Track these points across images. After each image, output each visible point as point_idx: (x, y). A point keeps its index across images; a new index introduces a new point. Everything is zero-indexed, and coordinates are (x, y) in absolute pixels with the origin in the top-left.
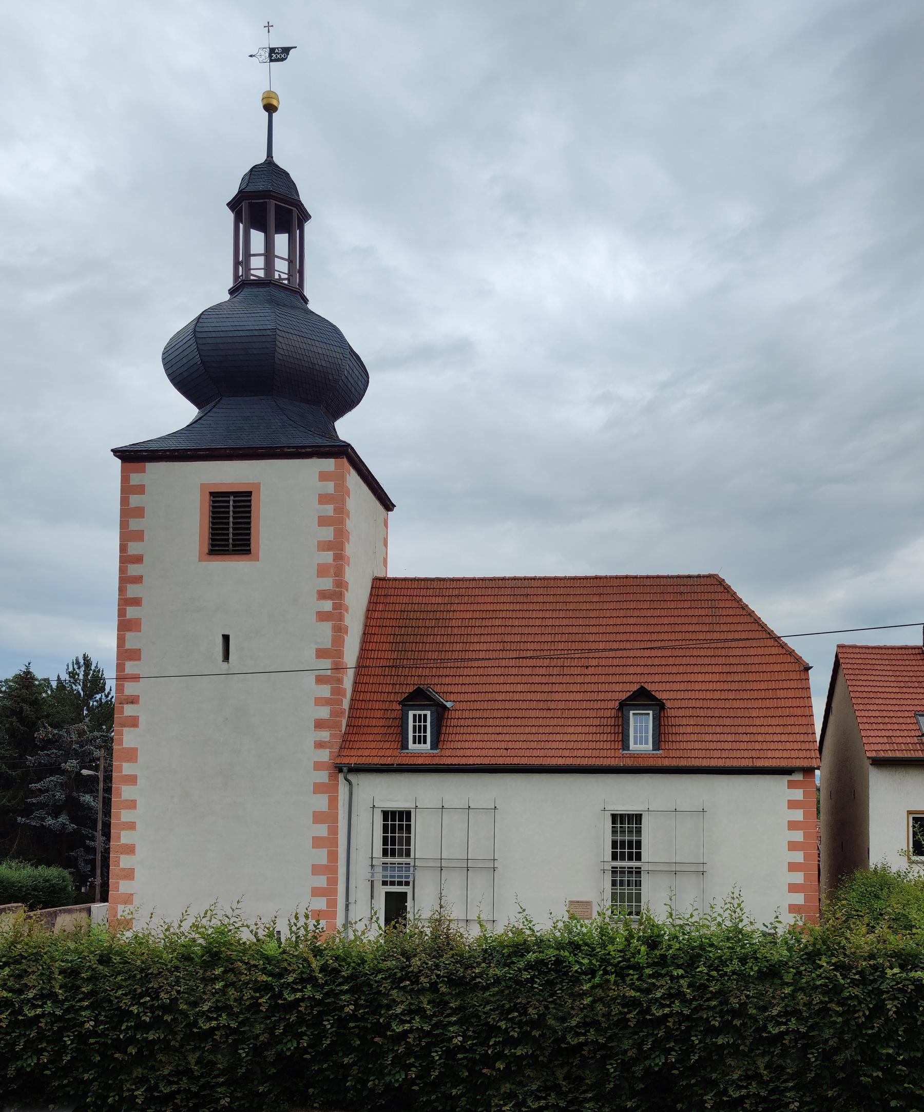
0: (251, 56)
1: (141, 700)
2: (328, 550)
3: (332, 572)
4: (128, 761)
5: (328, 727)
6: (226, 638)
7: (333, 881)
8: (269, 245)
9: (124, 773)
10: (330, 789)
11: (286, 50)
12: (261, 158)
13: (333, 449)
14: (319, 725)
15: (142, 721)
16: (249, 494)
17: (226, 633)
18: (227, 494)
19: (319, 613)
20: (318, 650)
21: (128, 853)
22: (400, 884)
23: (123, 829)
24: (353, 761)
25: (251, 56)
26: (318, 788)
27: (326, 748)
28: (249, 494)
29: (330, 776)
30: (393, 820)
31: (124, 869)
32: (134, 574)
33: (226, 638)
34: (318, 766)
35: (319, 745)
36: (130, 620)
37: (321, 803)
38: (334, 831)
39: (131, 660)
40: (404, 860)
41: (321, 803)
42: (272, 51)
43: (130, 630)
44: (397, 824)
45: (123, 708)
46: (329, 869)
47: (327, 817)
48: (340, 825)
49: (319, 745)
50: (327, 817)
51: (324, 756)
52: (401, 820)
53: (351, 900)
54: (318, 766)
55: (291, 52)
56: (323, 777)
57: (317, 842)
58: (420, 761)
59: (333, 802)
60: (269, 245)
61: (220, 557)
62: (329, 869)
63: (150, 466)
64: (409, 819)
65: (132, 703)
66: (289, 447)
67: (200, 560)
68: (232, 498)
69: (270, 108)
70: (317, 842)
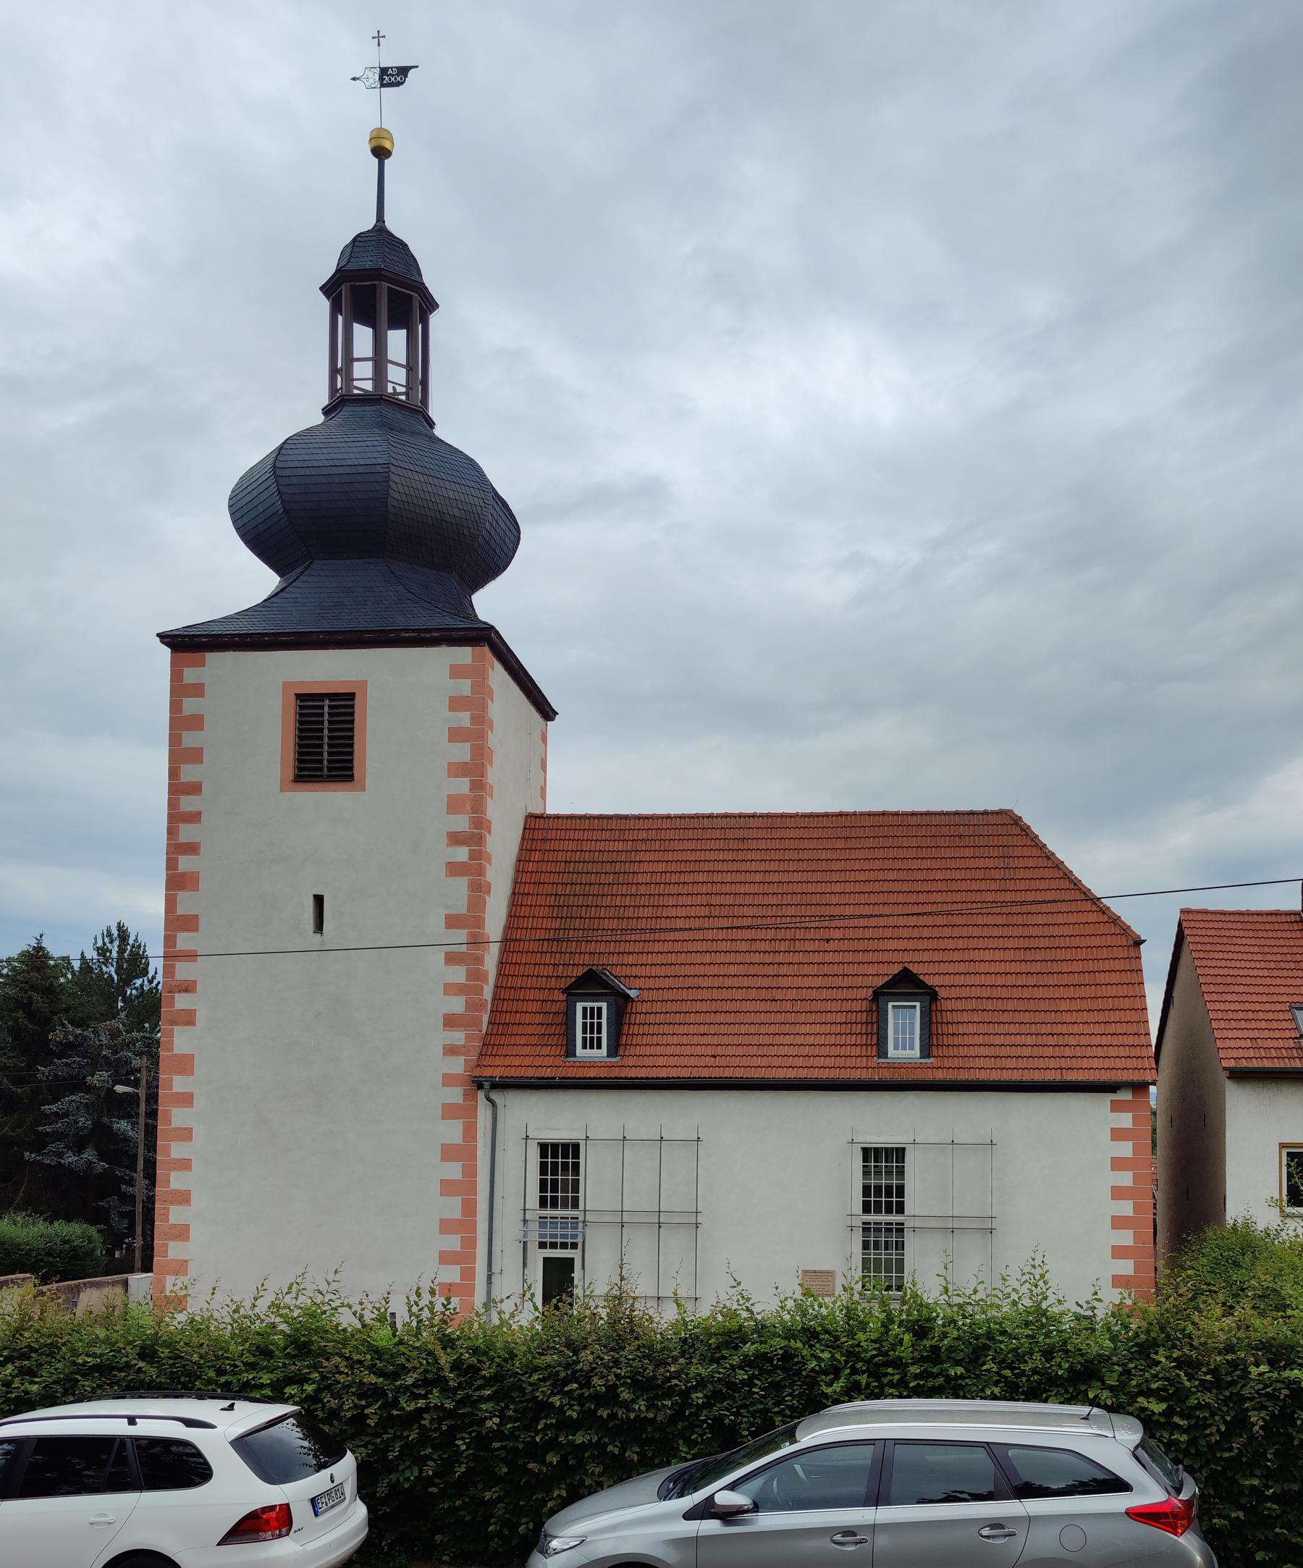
1: (199, 987)
2: (463, 776)
4: (180, 1073)
5: (462, 1026)
6: (319, 900)
7: (470, 1243)
8: (380, 346)
9: (175, 1090)
10: (465, 1113)
11: (404, 71)
12: (369, 223)
14: (450, 1022)
16: (352, 696)
17: (319, 893)
18: (320, 697)
19: (449, 864)
20: (448, 917)
21: (180, 1203)
22: (564, 1246)
23: (174, 1169)
24: (498, 1073)
26: (449, 1112)
27: (460, 1054)
28: (352, 696)
29: (466, 1094)
30: (555, 1156)
31: (174, 1226)
32: (189, 809)
33: (319, 900)
34: (448, 1080)
35: (450, 1050)
36: (183, 875)
37: (453, 1132)
38: (470, 1171)
39: (184, 930)
40: (569, 1213)
41: (453, 1132)
42: (384, 71)
43: (183, 888)
44: (560, 1162)
45: (173, 998)
46: (465, 1226)
47: (461, 1153)
48: (479, 1163)
49: (450, 1050)
50: (461, 1153)
51: (457, 1066)
52: (565, 1156)
53: (496, 1269)
54: (448, 1080)
55: (411, 73)
56: (455, 1095)
58: (592, 1073)
59: (470, 1131)
60: (380, 346)
61: (310, 785)
62: (465, 1226)
63: (213, 658)
64: (576, 1155)
65: (186, 991)
66: (407, 631)
67: (282, 790)
68: (327, 702)
69: (381, 153)
70: (447, 1187)
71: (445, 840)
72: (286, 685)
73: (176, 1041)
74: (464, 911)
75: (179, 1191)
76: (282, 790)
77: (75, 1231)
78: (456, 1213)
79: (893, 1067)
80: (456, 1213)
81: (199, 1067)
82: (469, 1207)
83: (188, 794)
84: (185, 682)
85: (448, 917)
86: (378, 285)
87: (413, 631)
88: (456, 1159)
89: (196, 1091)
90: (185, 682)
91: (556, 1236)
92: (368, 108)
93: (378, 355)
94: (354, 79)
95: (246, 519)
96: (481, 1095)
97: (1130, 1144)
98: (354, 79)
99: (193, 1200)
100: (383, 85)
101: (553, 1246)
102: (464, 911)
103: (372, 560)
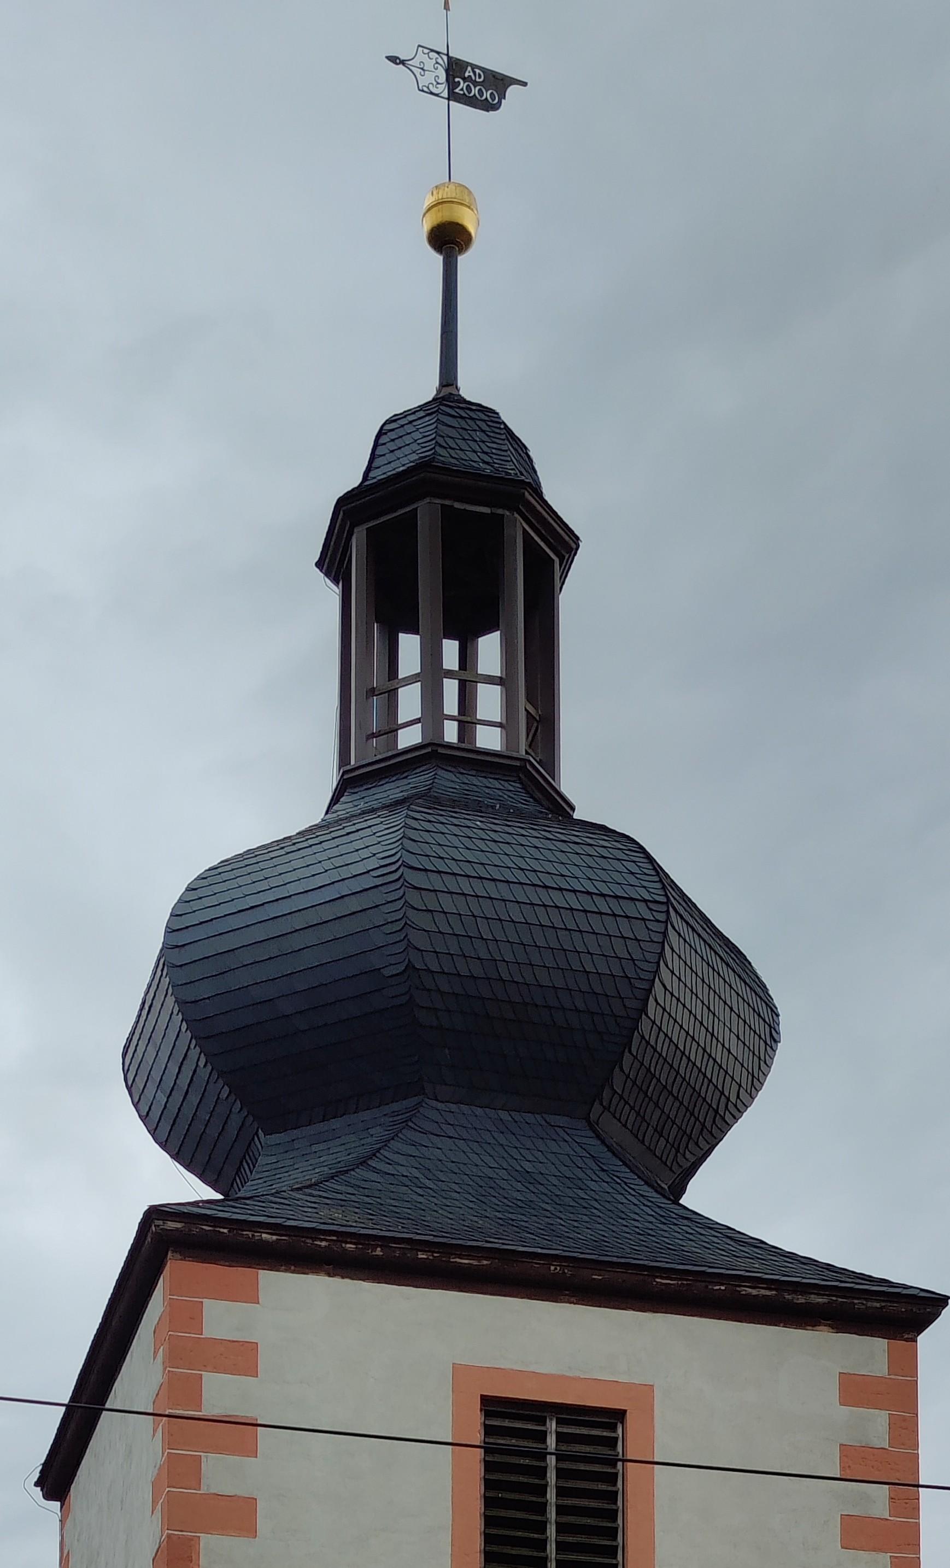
8: (467, 657)
11: (498, 84)
12: (425, 388)
19: (251, 1370)
42: (455, 68)
55: (512, 90)
66: (756, 1282)
68: (552, 1425)
69: (449, 239)
77: (528, 767)
84: (207, 1333)
85: (251, 1370)
86: (445, 535)
87: (770, 1284)
90: (207, 1333)
92: (424, 138)
93: (456, 691)
94: (393, 59)
95: (205, 990)
97: (209, 1331)
98: (393, 59)
100: (453, 96)
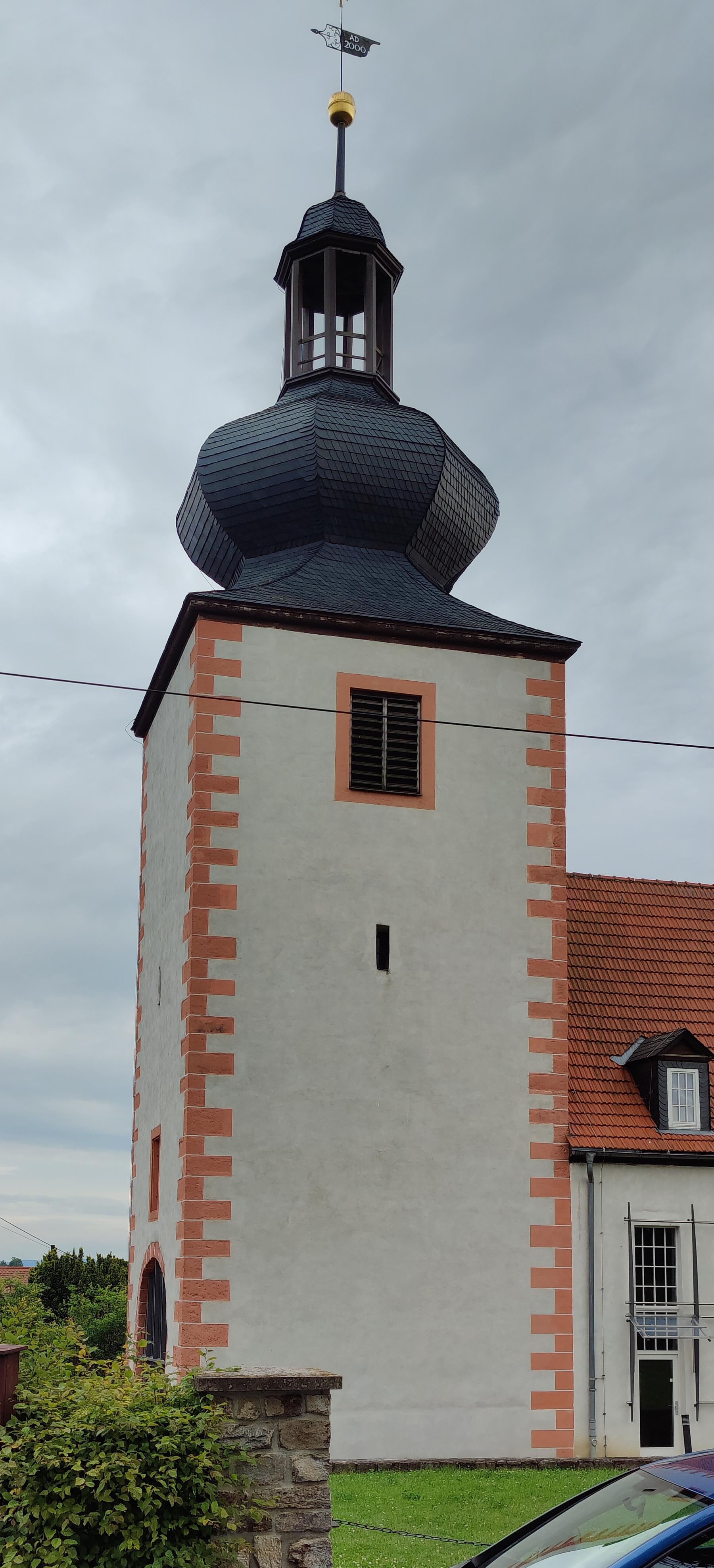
0: (315, 31)
1: (237, 1026)
2: (544, 804)
3: (550, 839)
4: (213, 1132)
5: (552, 1088)
6: (383, 934)
7: (565, 1344)
8: (347, 325)
9: (207, 1153)
10: (555, 1189)
11: (366, 43)
12: (328, 193)
13: (553, 647)
14: (537, 1083)
15: (239, 1063)
16: (419, 698)
17: (384, 923)
18: (378, 696)
19: (531, 902)
20: (531, 962)
21: (215, 1298)
22: (662, 1345)
23: (207, 1254)
24: (603, 1144)
25: (315, 31)
26: (538, 1188)
27: (549, 1121)
28: (419, 698)
29: (556, 1168)
30: (648, 1242)
31: (207, 1327)
32: (223, 808)
33: (383, 934)
34: (537, 1151)
35: (538, 1116)
36: (216, 888)
37: (544, 1211)
38: (564, 1259)
39: (217, 956)
40: (666, 1308)
41: (544, 1211)
42: (345, 36)
43: (216, 904)
44: (654, 1249)
45: (204, 1038)
46: (557, 1323)
47: (552, 1236)
48: (574, 1249)
49: (538, 1116)
50: (552, 1236)
51: (546, 1134)
52: (659, 1242)
53: (598, 1374)
54: (537, 1151)
55: (373, 47)
56: (545, 1168)
57: (539, 1277)
58: (686, 1147)
59: (563, 1211)
60: (347, 325)
61: (370, 796)
62: (557, 1323)
63: (250, 632)
64: (671, 1241)
65: (221, 1030)
66: (486, 633)
67: (337, 798)
68: (385, 703)
69: (341, 120)
70: (539, 1277)
71: (525, 875)
72: (341, 677)
73: (208, 1092)
74: (549, 956)
75: (214, 1282)
76: (337, 798)
78: (549, 1309)
79: (672, 1138)
80: (549, 1309)
81: (238, 1126)
82: (564, 1301)
83: (221, 790)
86: (338, 265)
88: (548, 1244)
89: (234, 1156)
91: (664, 1334)
92: (328, 74)
96: (577, 1173)
99: (232, 1293)
101: (650, 1345)
102: (549, 956)
103: (392, 553)
